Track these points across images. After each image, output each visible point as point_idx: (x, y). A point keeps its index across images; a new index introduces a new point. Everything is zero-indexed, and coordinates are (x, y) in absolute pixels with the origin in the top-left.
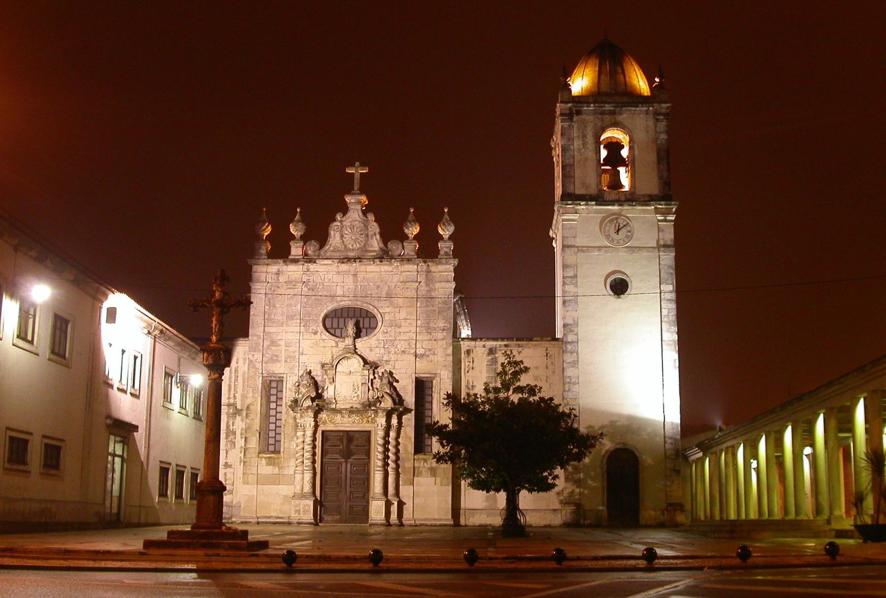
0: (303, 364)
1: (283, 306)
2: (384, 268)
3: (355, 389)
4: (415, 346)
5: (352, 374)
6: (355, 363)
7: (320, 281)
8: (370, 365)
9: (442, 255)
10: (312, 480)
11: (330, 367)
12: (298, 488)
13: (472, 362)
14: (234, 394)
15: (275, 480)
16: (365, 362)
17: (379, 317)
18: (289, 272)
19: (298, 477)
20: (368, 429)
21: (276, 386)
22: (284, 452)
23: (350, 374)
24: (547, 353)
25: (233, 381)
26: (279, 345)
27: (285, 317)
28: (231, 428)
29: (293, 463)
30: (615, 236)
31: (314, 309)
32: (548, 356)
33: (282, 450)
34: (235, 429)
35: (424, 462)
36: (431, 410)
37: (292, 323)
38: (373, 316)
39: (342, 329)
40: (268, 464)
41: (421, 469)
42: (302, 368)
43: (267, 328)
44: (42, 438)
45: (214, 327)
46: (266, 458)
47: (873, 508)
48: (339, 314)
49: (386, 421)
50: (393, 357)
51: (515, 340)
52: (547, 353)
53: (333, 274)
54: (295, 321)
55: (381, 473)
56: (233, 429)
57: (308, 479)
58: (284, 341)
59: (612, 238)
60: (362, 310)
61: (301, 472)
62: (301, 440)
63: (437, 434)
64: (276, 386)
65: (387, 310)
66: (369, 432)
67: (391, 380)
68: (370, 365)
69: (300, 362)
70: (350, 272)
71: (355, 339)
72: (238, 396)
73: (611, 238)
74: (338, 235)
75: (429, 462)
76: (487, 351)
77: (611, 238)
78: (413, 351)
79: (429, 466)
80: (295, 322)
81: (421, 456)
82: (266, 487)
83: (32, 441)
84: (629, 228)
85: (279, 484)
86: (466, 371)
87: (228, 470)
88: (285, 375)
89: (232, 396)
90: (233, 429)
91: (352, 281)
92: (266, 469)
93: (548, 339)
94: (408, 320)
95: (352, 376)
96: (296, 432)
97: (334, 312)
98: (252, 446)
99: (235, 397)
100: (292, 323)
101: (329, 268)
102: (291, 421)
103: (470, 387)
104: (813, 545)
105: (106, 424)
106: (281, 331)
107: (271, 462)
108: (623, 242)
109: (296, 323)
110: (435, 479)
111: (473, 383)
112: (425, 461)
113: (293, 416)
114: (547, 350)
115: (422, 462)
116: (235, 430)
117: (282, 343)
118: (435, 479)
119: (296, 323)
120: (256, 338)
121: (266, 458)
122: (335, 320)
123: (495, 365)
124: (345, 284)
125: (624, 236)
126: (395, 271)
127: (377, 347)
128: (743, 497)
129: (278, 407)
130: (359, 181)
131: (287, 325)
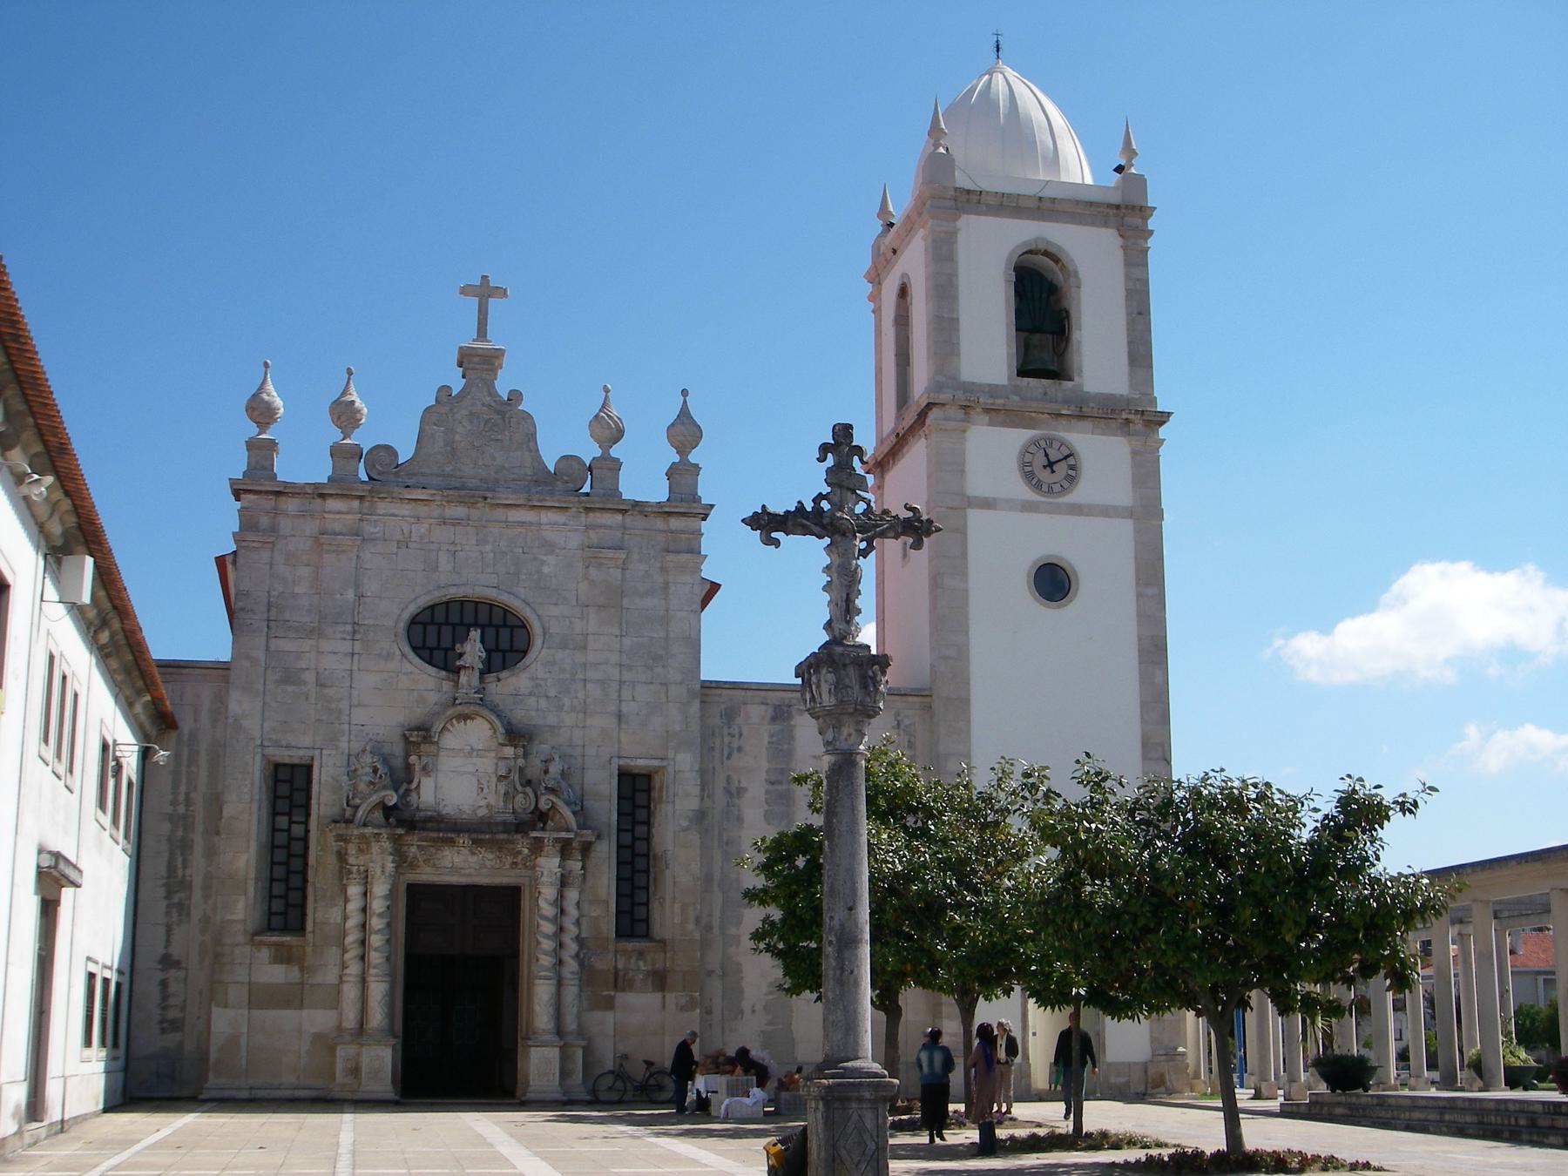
2: (547, 516)
3: (482, 789)
4: (616, 694)
6: (478, 732)
8: (516, 735)
10: (387, 998)
11: (420, 736)
13: (737, 736)
14: (187, 794)
15: (293, 997)
17: (536, 628)
18: (330, 512)
22: (313, 932)
24: (898, 721)
25: (185, 762)
26: (305, 683)
28: (180, 872)
29: (333, 953)
30: (1045, 475)
32: (902, 726)
34: (191, 876)
35: (637, 959)
36: (619, 847)
37: (334, 633)
41: (631, 974)
42: (356, 736)
43: (274, 640)
45: (687, 536)
46: (270, 945)
47: (401, 1035)
48: (440, 618)
52: (898, 721)
53: (431, 524)
55: (551, 984)
56: (184, 876)
57: (379, 997)
58: (314, 673)
59: (1039, 480)
60: (495, 609)
61: (345, 979)
68: (516, 735)
69: (353, 722)
70: (469, 520)
71: (482, 673)
72: (198, 797)
73: (1035, 480)
75: (649, 958)
76: (770, 712)
77: (1035, 480)
78: (612, 708)
80: (342, 629)
81: (631, 945)
82: (270, 1015)
84: (1071, 461)
85: (301, 1006)
86: (725, 755)
87: (172, 973)
88: (317, 752)
89: (182, 797)
90: (184, 876)
91: (474, 542)
94: (601, 637)
97: (429, 611)
98: (234, 917)
99: (188, 802)
101: (422, 510)
102: (332, 860)
103: (734, 790)
104: (773, 1109)
106: (307, 649)
107: (283, 956)
109: (343, 632)
110: (664, 996)
111: (739, 782)
112: (641, 954)
113: (335, 849)
114: (897, 714)
115: (634, 958)
116: (188, 879)
117: (310, 677)
121: (270, 945)
122: (432, 630)
123: (789, 744)
124: (458, 548)
125: (1063, 476)
126: (572, 523)
128: (550, 1027)
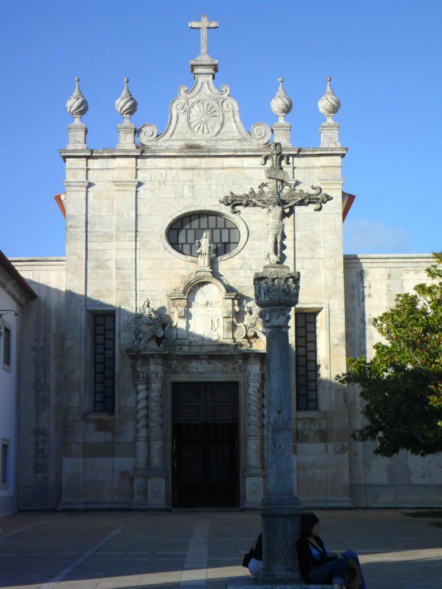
0: (142, 292)
1: (111, 214)
5: (209, 305)
7: (160, 179)
20: (235, 379)
21: (103, 323)
23: (208, 305)
27: (115, 229)
29: (130, 425)
33: (117, 409)
39: (191, 244)
40: (99, 429)
44: (223, 319)
64: (103, 323)
79: (317, 428)
83: (207, 307)
85: (113, 456)
92: (100, 437)
96: (136, 386)
105: (347, 151)
107: (102, 426)
109: (129, 237)
120: (75, 258)
127: (241, 268)
129: (304, 326)
130: (206, 40)
131: (118, 240)
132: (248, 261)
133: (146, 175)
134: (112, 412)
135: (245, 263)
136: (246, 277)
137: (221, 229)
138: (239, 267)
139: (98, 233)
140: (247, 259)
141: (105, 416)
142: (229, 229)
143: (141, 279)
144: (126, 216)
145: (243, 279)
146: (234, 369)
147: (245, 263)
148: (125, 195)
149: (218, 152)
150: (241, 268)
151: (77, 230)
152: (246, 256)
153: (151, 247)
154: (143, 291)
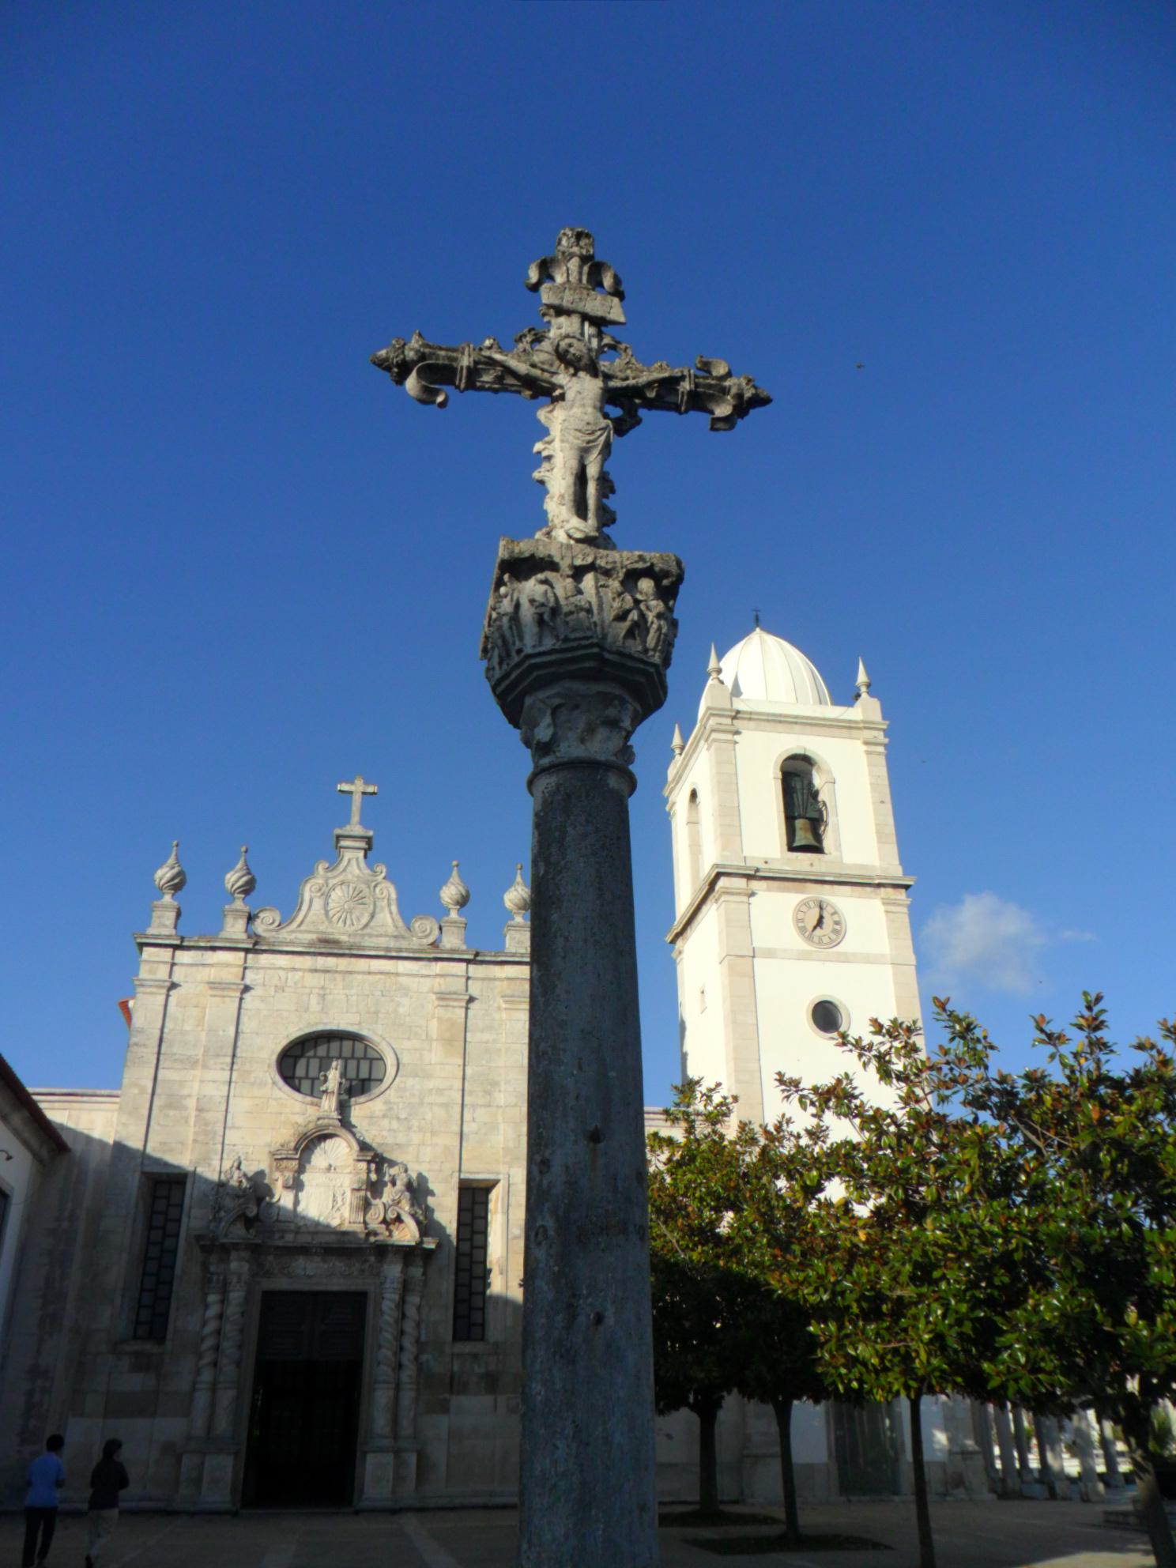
9: (906, 1495)
12: (199, 1422)
16: (364, 1147)
19: (202, 1399)
31: (708, 1228)
33: (170, 1335)
38: (378, 1056)
49: (402, 1272)
50: (416, 1138)
51: (838, 1433)
54: (221, 1060)
62: (212, 1311)
63: (718, 1237)
65: (407, 1044)
66: (363, 1295)
67: (418, 1191)
74: (318, 904)
79: (482, 1370)
92: (134, 1382)
93: (677, 740)
95: (332, 1175)
96: (205, 1295)
100: (215, 1064)
107: (143, 1364)
108: (828, 940)
109: (222, 1063)
110: (495, 1400)
117: (191, 1103)
118: (495, 1400)
119: (222, 1063)
120: (136, 1091)
127: (384, 1116)
132: (395, 1107)
133: (257, 977)
134: (161, 1340)
135: (390, 1109)
136: (390, 1130)
137: (359, 1060)
138: (381, 1114)
139: (177, 1057)
140: (394, 1103)
141: (149, 1347)
142: (371, 1060)
143: (245, 968)
144: (221, 1033)
145: (385, 1133)
146: (362, 1271)
147: (390, 1109)
148: (224, 1002)
149: (364, 950)
150: (384, 1116)
151: (145, 1050)
152: (393, 1099)
153: (252, 1080)
154: (234, 1145)
